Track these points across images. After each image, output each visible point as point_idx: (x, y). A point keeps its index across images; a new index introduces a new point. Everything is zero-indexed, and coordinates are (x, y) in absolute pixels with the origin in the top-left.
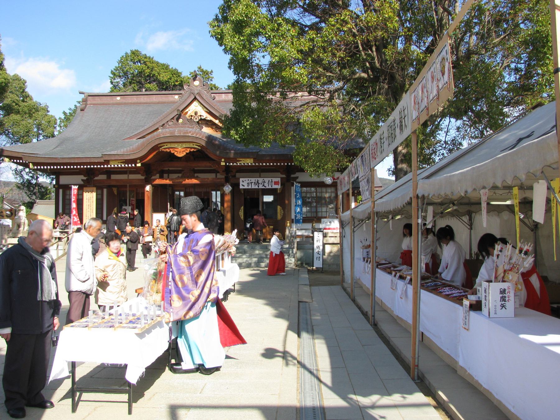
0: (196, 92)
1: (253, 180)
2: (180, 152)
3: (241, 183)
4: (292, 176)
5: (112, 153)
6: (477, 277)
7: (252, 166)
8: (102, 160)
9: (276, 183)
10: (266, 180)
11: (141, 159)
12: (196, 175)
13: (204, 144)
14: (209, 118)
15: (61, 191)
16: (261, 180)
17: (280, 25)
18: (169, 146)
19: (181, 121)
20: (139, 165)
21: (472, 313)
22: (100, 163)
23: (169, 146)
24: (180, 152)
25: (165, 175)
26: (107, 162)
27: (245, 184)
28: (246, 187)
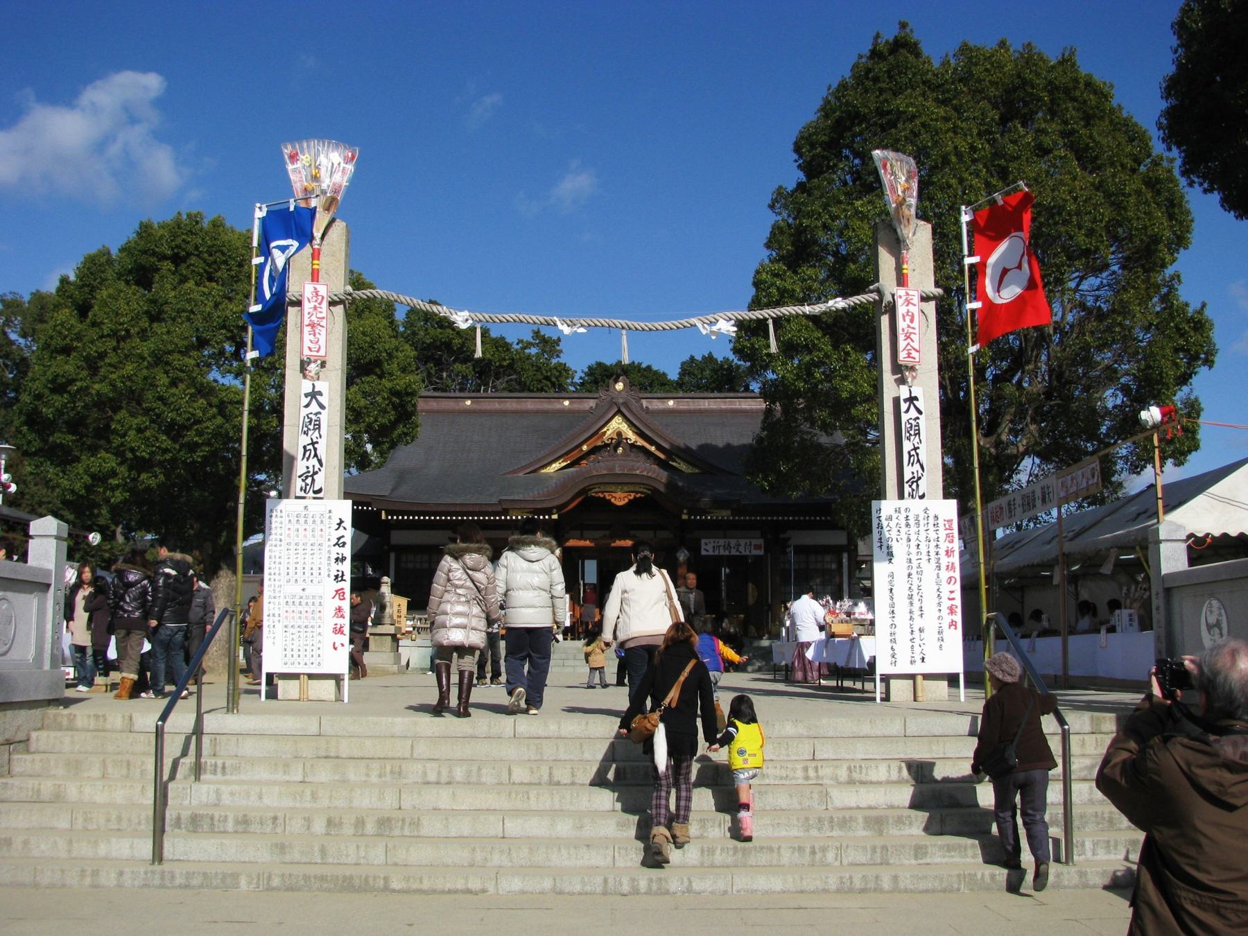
0: (621, 401)
1: (722, 542)
2: (620, 499)
3: (703, 546)
4: (782, 536)
5: (516, 497)
6: (1045, 811)
7: (728, 520)
8: (499, 509)
9: (757, 547)
10: (742, 542)
11: (559, 508)
12: (632, 532)
13: (662, 489)
14: (641, 442)
15: (392, 556)
16: (733, 542)
17: (847, 354)
18: (603, 488)
19: (620, 450)
20: (555, 517)
21: (1110, 635)
22: (495, 514)
23: (603, 488)
24: (620, 499)
25: (586, 533)
26: (505, 512)
27: (710, 547)
28: (711, 553)
